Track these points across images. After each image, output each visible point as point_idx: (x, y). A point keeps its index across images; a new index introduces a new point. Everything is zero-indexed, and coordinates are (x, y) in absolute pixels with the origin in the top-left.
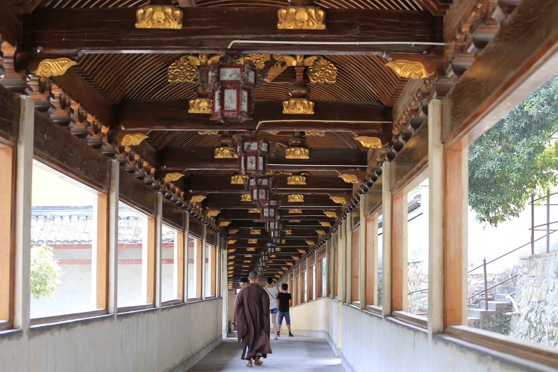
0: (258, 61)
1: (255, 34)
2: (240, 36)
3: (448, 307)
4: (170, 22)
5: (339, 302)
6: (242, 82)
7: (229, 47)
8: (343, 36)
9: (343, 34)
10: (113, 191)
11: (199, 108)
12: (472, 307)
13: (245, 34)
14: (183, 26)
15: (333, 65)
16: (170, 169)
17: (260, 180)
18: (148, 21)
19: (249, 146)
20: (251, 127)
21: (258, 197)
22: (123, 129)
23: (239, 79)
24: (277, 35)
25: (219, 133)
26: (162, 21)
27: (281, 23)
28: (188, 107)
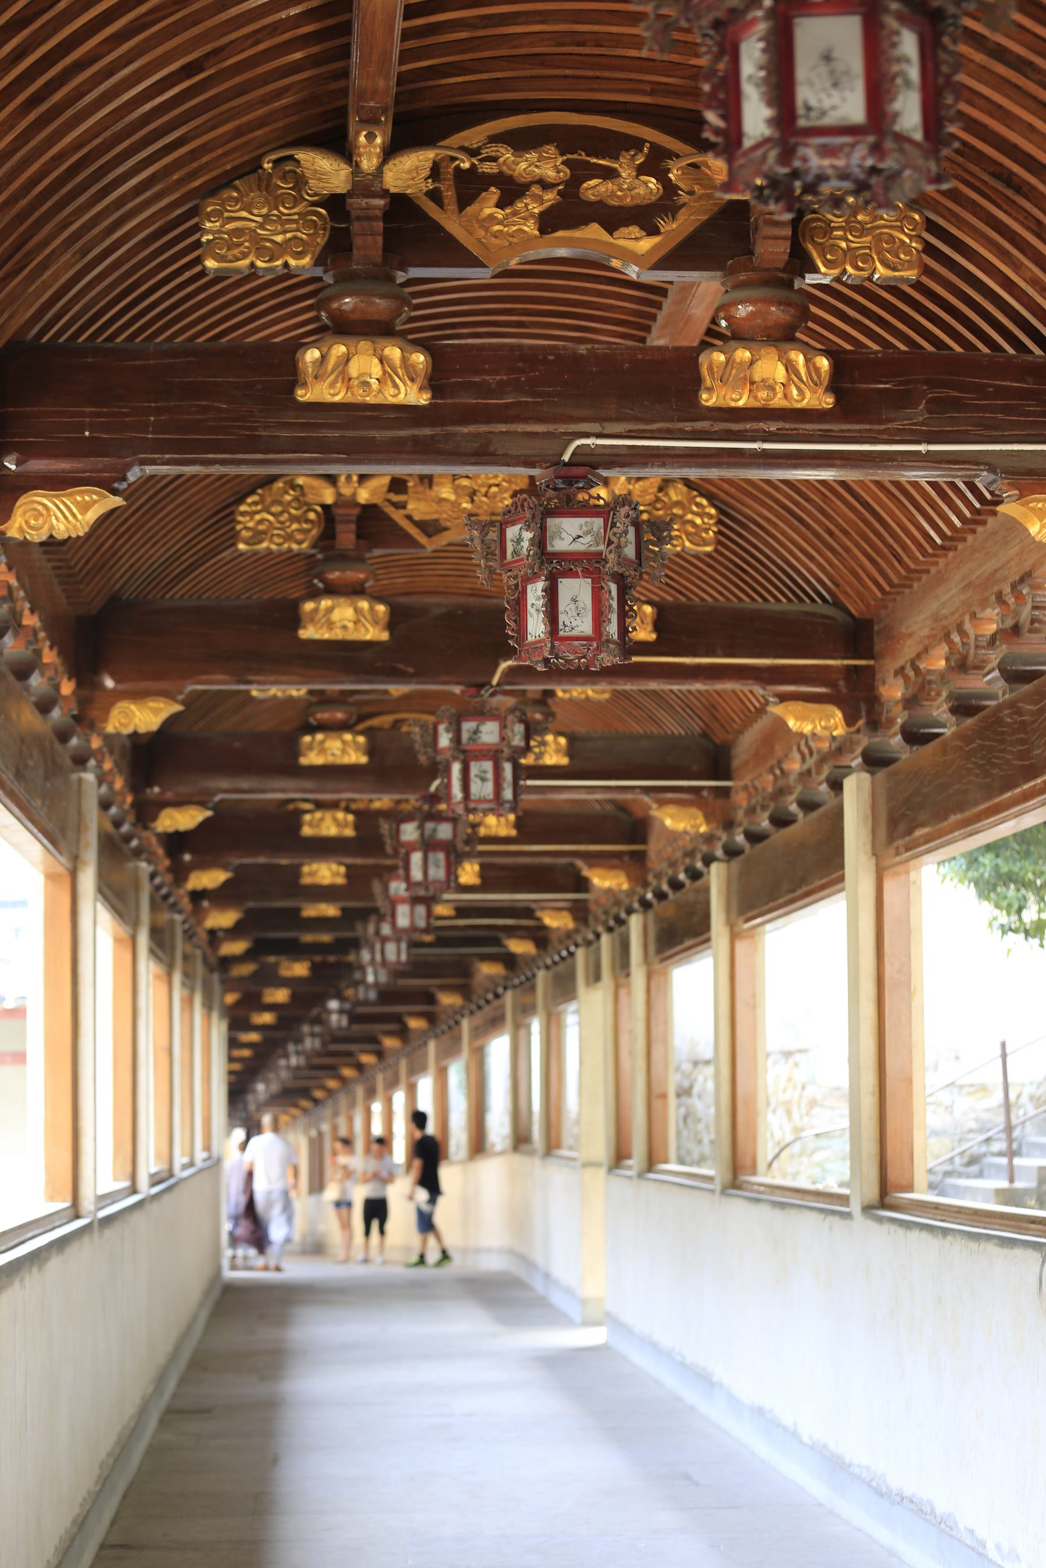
0: (494, 489)
1: (638, 419)
2: (595, 427)
3: (892, 1175)
4: (396, 386)
5: (586, 1165)
6: (611, 557)
7: (566, 457)
8: (882, 427)
9: (880, 422)
10: (85, 863)
11: (330, 625)
12: (960, 1175)
13: (609, 420)
14: (433, 397)
15: (704, 502)
16: (169, 795)
17: (429, 826)
18: (335, 382)
19: (476, 732)
20: (480, 680)
21: (425, 873)
22: (109, 683)
23: (602, 547)
24: (699, 425)
25: (311, 692)
26: (373, 381)
27: (710, 390)
28: (295, 621)
